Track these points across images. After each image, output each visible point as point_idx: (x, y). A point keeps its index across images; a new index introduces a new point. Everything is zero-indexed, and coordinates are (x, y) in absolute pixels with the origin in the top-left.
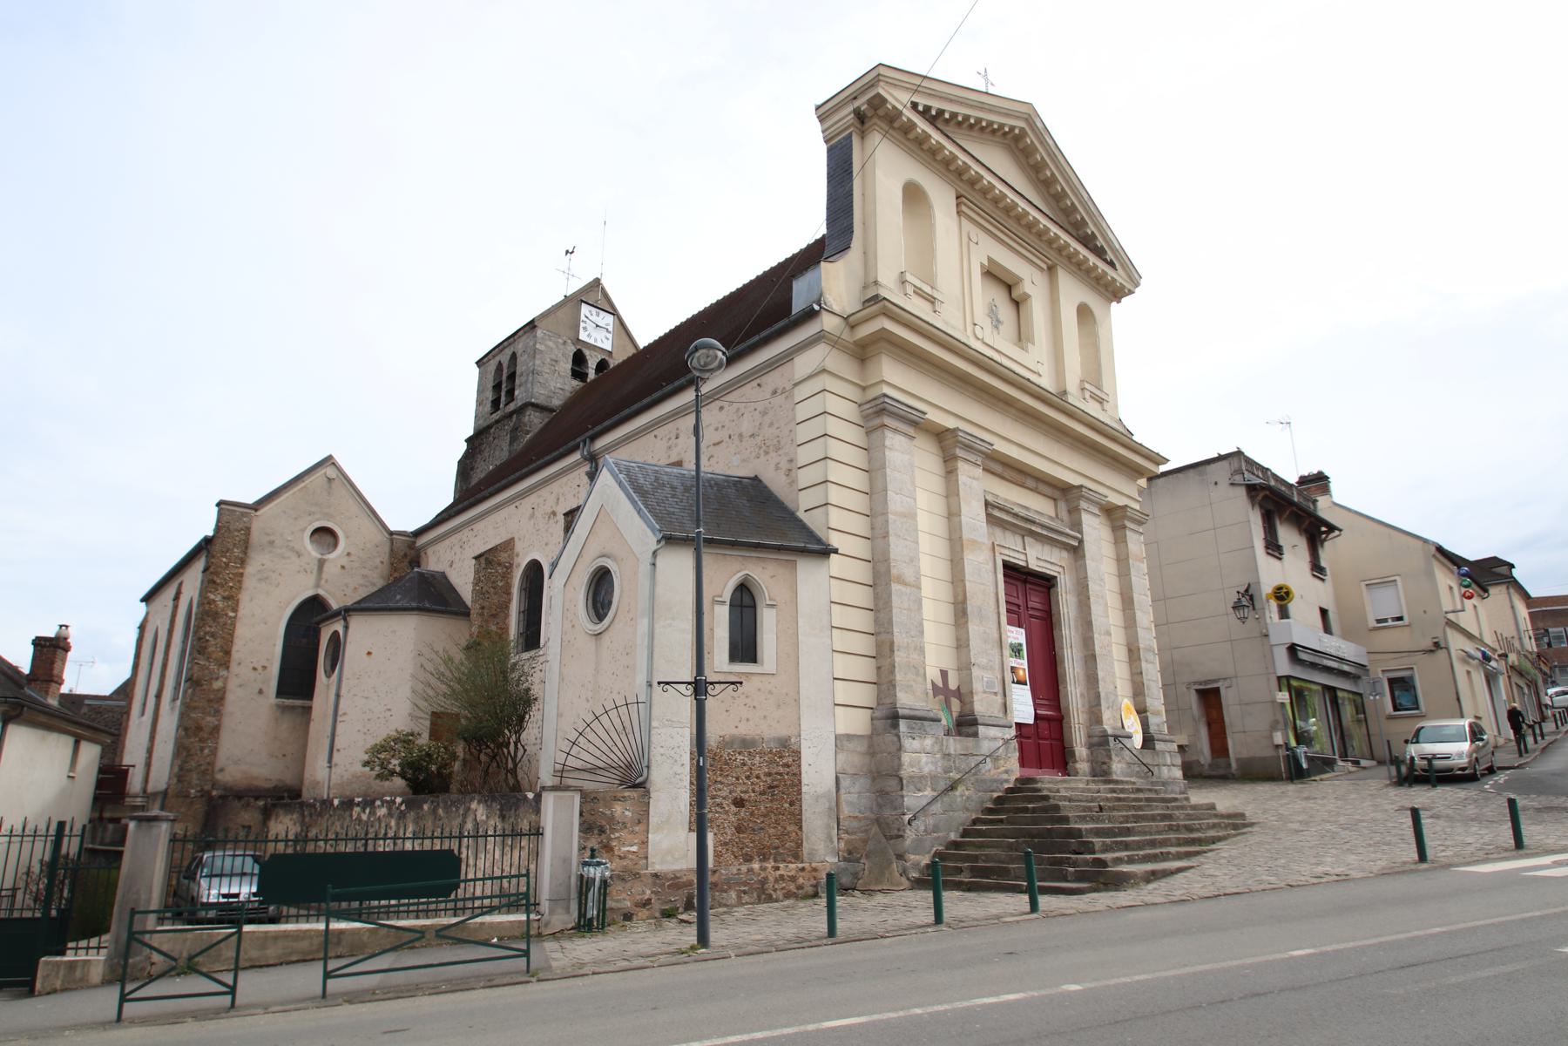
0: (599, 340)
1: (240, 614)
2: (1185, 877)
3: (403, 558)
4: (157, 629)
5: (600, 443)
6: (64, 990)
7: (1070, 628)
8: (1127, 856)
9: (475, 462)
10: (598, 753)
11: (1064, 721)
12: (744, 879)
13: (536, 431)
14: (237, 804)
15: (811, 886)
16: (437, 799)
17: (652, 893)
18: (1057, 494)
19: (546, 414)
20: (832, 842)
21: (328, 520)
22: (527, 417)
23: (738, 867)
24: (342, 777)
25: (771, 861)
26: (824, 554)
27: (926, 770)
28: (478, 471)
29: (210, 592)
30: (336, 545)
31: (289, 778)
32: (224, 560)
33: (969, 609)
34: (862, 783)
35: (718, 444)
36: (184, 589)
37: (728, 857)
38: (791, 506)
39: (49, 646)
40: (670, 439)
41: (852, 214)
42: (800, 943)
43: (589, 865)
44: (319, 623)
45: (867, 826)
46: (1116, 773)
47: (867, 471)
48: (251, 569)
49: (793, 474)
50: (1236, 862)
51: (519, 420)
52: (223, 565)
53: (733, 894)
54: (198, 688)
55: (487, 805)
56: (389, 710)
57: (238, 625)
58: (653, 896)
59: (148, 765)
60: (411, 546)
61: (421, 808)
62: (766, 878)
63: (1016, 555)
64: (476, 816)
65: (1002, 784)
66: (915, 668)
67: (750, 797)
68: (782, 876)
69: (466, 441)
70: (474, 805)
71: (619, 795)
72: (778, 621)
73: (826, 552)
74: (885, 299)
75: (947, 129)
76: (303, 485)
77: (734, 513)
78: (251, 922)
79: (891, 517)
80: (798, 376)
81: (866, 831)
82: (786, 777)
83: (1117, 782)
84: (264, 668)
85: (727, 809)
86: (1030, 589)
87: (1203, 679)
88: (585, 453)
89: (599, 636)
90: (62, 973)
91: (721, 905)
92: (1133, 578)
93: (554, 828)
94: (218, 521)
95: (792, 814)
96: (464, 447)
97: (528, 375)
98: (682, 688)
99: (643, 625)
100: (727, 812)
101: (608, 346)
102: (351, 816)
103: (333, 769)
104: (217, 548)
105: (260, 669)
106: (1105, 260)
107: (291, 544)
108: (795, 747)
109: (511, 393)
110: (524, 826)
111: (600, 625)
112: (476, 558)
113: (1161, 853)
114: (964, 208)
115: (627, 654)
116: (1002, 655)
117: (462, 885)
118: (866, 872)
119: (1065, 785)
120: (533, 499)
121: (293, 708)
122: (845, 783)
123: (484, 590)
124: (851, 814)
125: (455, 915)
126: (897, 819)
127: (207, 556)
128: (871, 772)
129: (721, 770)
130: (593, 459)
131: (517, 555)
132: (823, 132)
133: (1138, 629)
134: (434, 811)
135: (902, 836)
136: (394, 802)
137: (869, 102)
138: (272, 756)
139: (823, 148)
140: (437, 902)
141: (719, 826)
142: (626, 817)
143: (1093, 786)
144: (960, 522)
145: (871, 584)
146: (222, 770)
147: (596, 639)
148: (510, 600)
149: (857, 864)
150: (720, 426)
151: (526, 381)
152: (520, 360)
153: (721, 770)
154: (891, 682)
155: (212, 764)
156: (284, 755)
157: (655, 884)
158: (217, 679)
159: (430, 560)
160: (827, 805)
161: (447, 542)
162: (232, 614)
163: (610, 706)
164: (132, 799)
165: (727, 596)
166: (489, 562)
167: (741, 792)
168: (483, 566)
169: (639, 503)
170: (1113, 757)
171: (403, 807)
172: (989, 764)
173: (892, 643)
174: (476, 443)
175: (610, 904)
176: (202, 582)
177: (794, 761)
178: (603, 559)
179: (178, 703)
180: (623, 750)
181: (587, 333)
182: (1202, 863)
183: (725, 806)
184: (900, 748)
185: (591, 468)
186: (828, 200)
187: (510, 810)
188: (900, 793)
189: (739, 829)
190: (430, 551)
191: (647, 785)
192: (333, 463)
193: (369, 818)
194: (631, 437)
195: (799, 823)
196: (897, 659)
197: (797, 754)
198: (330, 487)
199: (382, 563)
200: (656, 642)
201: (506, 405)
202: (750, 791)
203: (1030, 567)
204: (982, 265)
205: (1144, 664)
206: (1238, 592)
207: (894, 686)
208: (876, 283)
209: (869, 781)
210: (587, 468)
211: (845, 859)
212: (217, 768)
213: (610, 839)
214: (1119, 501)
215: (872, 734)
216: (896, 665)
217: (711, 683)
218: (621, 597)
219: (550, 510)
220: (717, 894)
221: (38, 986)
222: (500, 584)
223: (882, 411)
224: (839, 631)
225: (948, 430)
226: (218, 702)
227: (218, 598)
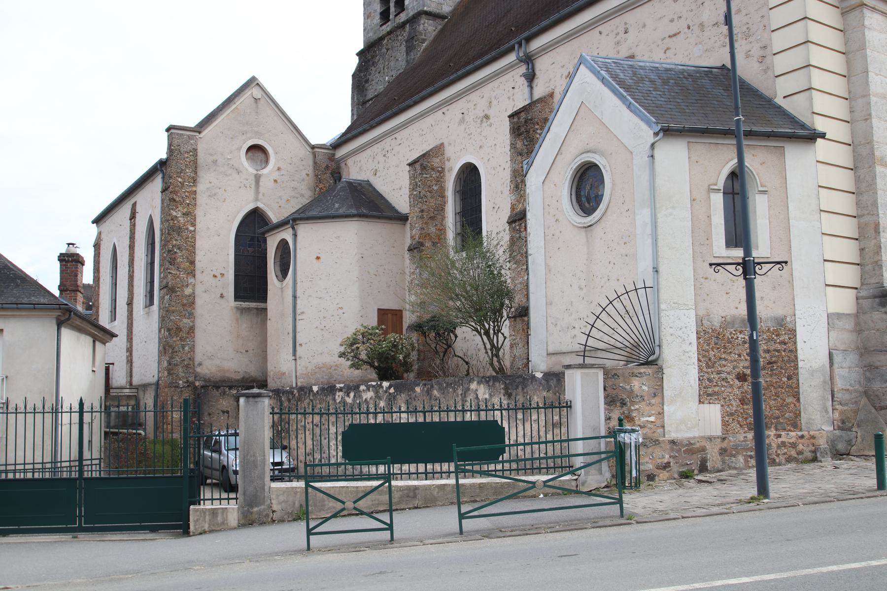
1: (197, 227)
3: (325, 169)
4: (114, 244)
5: (536, 44)
6: (211, 531)
9: (370, 74)
12: (750, 445)
13: (431, 38)
14: (215, 393)
15: (810, 451)
16: (430, 382)
17: (670, 457)
19: (438, 21)
20: (827, 411)
21: (259, 138)
22: (422, 26)
23: (744, 435)
24: (307, 368)
25: (772, 429)
26: (811, 139)
28: (374, 82)
29: (172, 209)
30: (267, 161)
31: (253, 370)
32: (180, 180)
34: (853, 358)
35: (675, 35)
36: (138, 209)
37: (735, 425)
38: (767, 93)
39: (72, 261)
40: (617, 34)
42: (852, 495)
43: (625, 432)
44: (264, 233)
45: (857, 397)
47: (844, 53)
48: (201, 187)
49: (768, 61)
51: (414, 30)
52: (179, 184)
53: (741, 459)
54: (174, 295)
55: (489, 386)
56: (341, 308)
57: (197, 237)
58: (671, 460)
59: (130, 361)
60: (331, 158)
61: (413, 390)
64: (477, 395)
68: (783, 443)
69: (358, 54)
70: (473, 386)
71: (636, 371)
72: (770, 207)
73: (812, 136)
76: (234, 106)
77: (715, 102)
78: (200, 496)
79: (873, 99)
81: (856, 402)
82: (783, 353)
84: (222, 275)
85: (731, 383)
88: (521, 54)
90: (207, 518)
91: (730, 468)
93: (584, 401)
94: (170, 145)
95: (790, 387)
96: (356, 60)
98: (731, 268)
99: (644, 215)
100: (731, 386)
102: (334, 399)
103: (298, 361)
104: (172, 169)
105: (219, 276)
107: (231, 162)
108: (790, 326)
112: (409, 165)
117: (507, 449)
118: (859, 439)
120: (461, 105)
121: (249, 310)
122: (837, 358)
124: (844, 387)
125: (547, 474)
127: (163, 178)
128: (858, 348)
129: (725, 348)
130: (529, 60)
131: (449, 160)
134: (429, 393)
136: (381, 386)
138: (237, 352)
140: (472, 465)
141: (725, 399)
142: (643, 390)
145: (852, 167)
146: (200, 364)
147: (586, 231)
149: (849, 433)
150: (675, 17)
153: (725, 348)
154: (876, 262)
155: (192, 359)
156: (247, 351)
157: (672, 450)
158: (187, 286)
159: (351, 170)
160: (822, 379)
161: (369, 152)
162: (192, 228)
164: (115, 390)
165: (721, 185)
166: (424, 168)
167: (743, 367)
168: (419, 171)
169: (628, 97)
171: (392, 390)
173: (877, 225)
174: (369, 56)
176: (163, 201)
177: (790, 339)
178: (590, 154)
179: (155, 307)
183: (729, 380)
185: (528, 69)
187: (517, 388)
190: (350, 162)
191: (659, 362)
192: (258, 84)
193: (354, 400)
194: (572, 35)
195: (797, 396)
196: (882, 240)
197: (793, 332)
198: (257, 107)
199: (308, 175)
200: (659, 231)
201: (396, 16)
207: (881, 267)
209: (857, 357)
210: (523, 69)
211: (840, 428)
212: (196, 363)
213: (630, 411)
215: (858, 313)
216: (882, 245)
217: (759, 264)
218: (613, 189)
219: (482, 114)
220: (727, 458)
221: (192, 528)
222: (435, 188)
224: (826, 214)
226: (190, 306)
227: (179, 215)
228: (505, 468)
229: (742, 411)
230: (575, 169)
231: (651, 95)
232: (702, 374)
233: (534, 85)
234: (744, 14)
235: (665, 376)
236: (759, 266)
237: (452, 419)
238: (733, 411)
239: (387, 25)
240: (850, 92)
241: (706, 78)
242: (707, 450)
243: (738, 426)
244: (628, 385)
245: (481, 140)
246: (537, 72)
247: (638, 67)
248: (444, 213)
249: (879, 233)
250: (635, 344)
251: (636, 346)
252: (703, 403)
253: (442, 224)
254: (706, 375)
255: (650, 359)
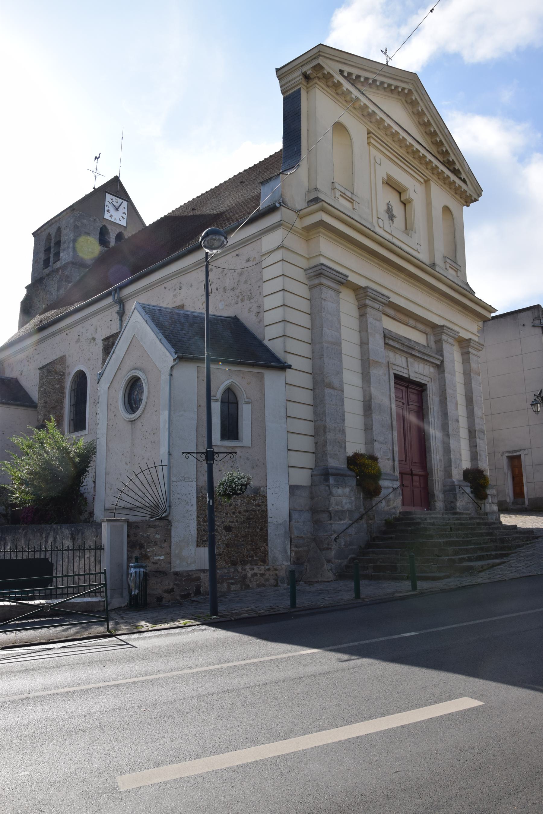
0: (118, 219)
2: (501, 568)
5: (126, 292)
7: (434, 418)
8: (468, 557)
10: (136, 497)
11: (429, 476)
18: (428, 330)
20: (286, 552)
27: (347, 507)
33: (373, 406)
38: (259, 336)
40: (175, 290)
41: (301, 143)
46: (459, 508)
50: (529, 558)
58: (175, 587)
62: (246, 576)
63: (402, 370)
65: (391, 515)
66: (339, 443)
67: (235, 525)
73: (283, 367)
74: (323, 201)
75: (362, 88)
80: (264, 250)
83: (460, 513)
85: (221, 532)
86: (410, 392)
87: (511, 449)
88: (116, 298)
89: (133, 422)
92: (473, 386)
97: (69, 243)
101: (124, 223)
106: (460, 178)
109: (57, 254)
110: (90, 543)
111: (134, 415)
112: (40, 369)
113: (487, 555)
114: (372, 141)
115: (154, 434)
116: (392, 435)
117: (54, 580)
118: (308, 570)
119: (429, 516)
122: (295, 516)
123: (46, 390)
124: (299, 535)
126: (327, 538)
130: (121, 302)
131: (68, 367)
132: (281, 87)
133: (475, 418)
135: (330, 548)
137: (314, 68)
139: (281, 97)
143: (445, 516)
144: (368, 349)
145: (312, 388)
148: (64, 398)
151: (68, 247)
152: (64, 232)
160: (284, 530)
163: (144, 467)
167: (230, 522)
170: (458, 498)
172: (384, 503)
173: (325, 427)
175: (149, 591)
177: (262, 502)
180: (153, 495)
181: (110, 214)
182: (510, 560)
184: (331, 493)
185: (120, 308)
186: (284, 133)
188: (329, 522)
189: (227, 545)
194: (148, 288)
195: (266, 540)
197: (265, 497)
201: (54, 263)
202: (235, 521)
203: (411, 378)
204: (383, 179)
205: (478, 440)
206: (535, 395)
208: (316, 189)
214: (466, 335)
215: (312, 485)
216: (327, 441)
217: (217, 453)
218: (148, 396)
219: (90, 337)
222: (57, 386)
223: (319, 275)
225: (361, 288)
228: (69, 593)
229: (227, 552)
230: (127, 380)
231: (178, 333)
232: (200, 527)
233: (123, 319)
234: (249, 284)
235: (172, 528)
236: (216, 455)
237: (19, 557)
238: (221, 552)
239: (47, 269)
240: (312, 340)
241: (221, 324)
242: (201, 579)
243: (224, 562)
244: (145, 534)
245: (89, 355)
246: (126, 311)
247: (174, 314)
248: (62, 404)
249: (326, 432)
250: (157, 505)
251: (157, 506)
252: (200, 547)
253: (60, 413)
254: (203, 527)
255: (163, 516)
